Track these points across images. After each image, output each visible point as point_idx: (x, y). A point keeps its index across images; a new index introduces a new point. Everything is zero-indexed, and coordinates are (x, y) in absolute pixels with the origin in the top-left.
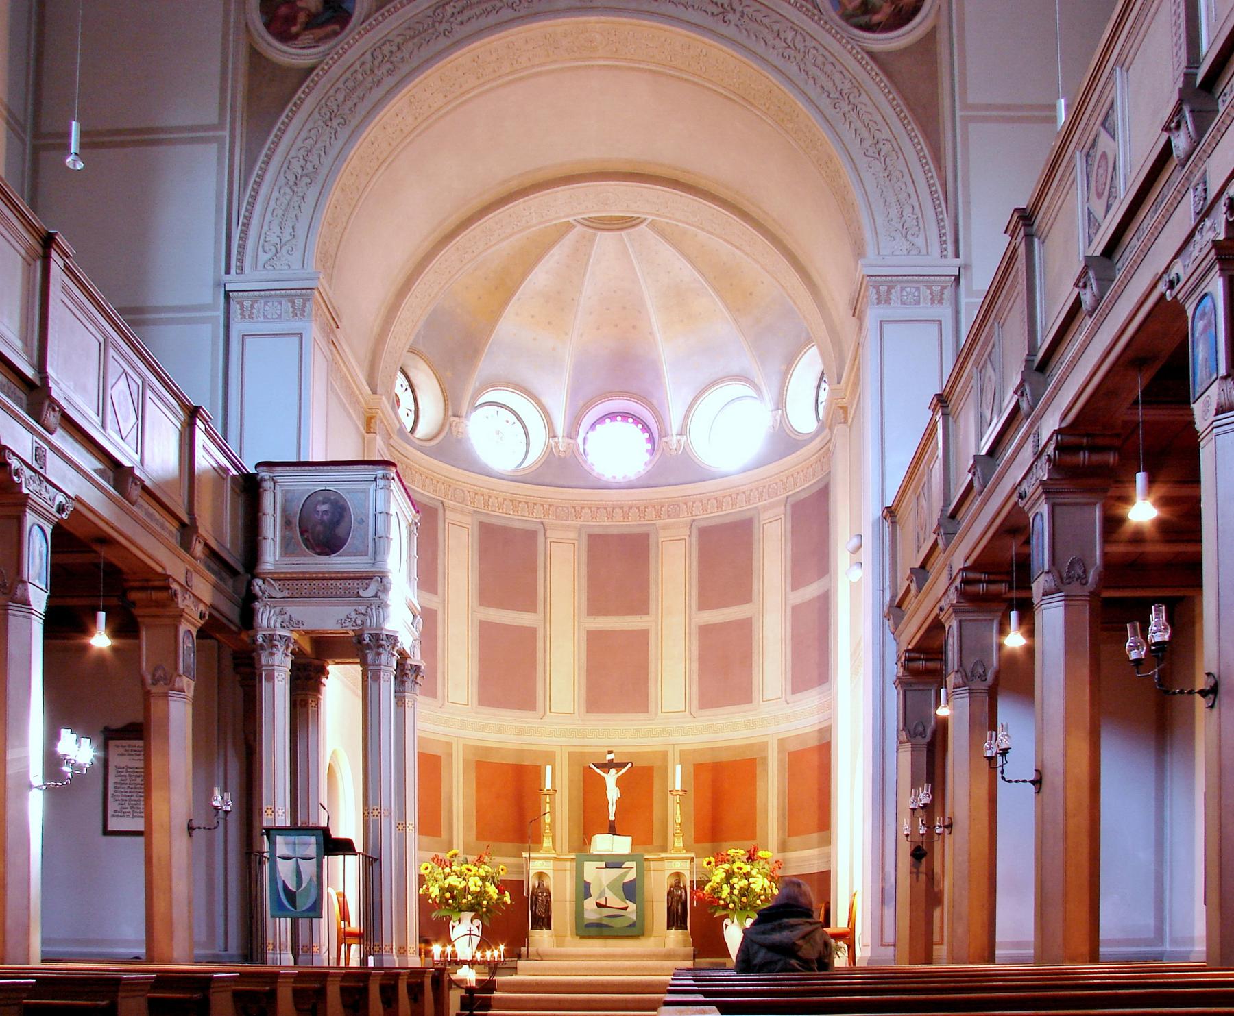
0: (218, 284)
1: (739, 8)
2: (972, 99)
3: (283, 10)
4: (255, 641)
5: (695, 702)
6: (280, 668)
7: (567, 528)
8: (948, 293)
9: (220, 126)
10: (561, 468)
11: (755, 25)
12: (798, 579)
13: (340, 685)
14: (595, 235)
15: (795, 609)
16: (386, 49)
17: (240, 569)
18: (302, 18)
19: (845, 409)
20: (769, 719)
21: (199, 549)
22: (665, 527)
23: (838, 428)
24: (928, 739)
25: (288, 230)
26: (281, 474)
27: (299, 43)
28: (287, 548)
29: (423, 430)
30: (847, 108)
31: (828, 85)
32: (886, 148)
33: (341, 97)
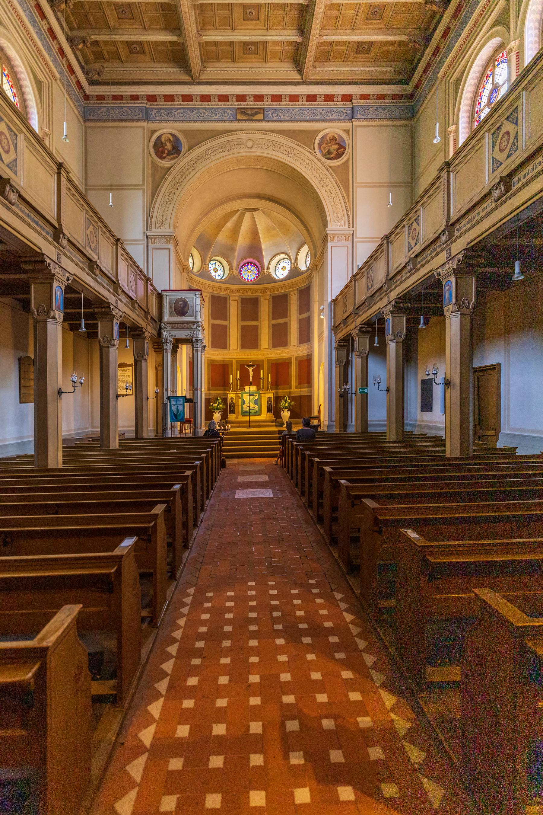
0: (144, 233)
1: (293, 153)
2: (358, 180)
3: (161, 149)
4: (162, 341)
5: (271, 346)
6: (169, 347)
7: (235, 296)
8: (351, 238)
9: (143, 185)
10: (234, 279)
11: (297, 158)
12: (300, 312)
13: (184, 351)
14: (461, 454)
15: (300, 320)
16: (192, 163)
17: (157, 321)
18: (166, 152)
19: (316, 266)
20: (293, 350)
21: (149, 318)
22: (263, 296)
23: (315, 273)
24: (344, 364)
25: (164, 218)
26: (169, 293)
27: (166, 159)
28: (171, 314)
29: (195, 270)
30: (323, 183)
31: (318, 176)
32: (334, 195)
33: (179, 177)
